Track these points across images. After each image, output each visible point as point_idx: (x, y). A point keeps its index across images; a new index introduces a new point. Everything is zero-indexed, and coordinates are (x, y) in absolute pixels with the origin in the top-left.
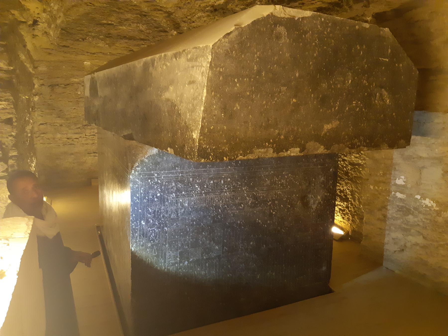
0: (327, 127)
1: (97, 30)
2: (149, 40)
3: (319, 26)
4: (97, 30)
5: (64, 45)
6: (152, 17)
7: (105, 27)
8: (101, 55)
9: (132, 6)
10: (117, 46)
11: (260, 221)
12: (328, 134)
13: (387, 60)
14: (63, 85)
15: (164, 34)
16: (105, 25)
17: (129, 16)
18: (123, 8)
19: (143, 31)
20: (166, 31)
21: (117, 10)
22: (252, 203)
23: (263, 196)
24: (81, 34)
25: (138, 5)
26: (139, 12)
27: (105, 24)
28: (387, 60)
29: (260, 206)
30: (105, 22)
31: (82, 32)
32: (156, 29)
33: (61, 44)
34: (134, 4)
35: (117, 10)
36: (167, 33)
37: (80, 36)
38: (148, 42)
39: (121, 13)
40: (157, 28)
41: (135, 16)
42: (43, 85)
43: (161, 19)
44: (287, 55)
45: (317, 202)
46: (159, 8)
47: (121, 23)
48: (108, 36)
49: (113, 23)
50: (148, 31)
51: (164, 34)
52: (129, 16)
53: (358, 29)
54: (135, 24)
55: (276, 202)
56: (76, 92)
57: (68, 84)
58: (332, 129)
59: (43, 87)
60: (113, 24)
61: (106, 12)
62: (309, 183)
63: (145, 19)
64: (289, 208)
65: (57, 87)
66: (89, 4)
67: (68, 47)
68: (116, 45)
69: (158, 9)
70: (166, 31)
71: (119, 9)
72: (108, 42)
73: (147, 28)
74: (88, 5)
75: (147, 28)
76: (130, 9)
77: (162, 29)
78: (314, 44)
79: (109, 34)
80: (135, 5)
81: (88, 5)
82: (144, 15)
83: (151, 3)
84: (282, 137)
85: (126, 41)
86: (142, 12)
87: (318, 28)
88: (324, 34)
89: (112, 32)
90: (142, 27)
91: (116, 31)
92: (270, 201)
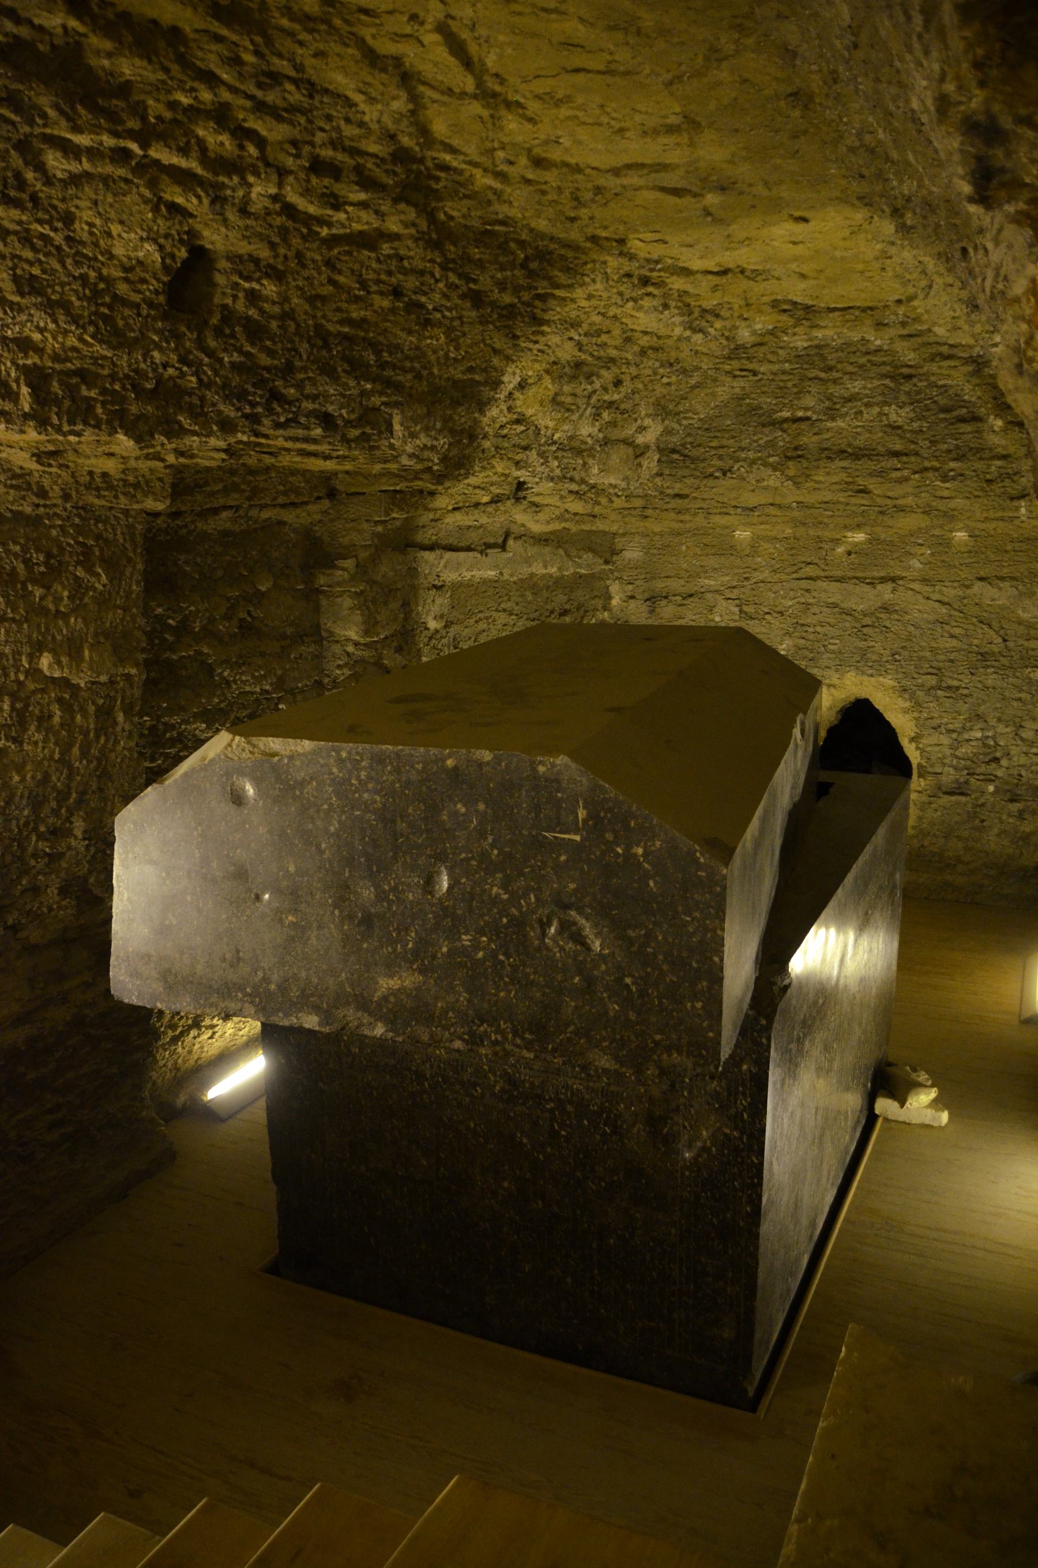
0: (386, 984)
1: (761, 442)
2: (917, 454)
3: (335, 770)
4: (761, 442)
5: (676, 491)
6: (932, 379)
7: (784, 431)
8: (772, 511)
9: (867, 353)
10: (818, 482)
11: (525, 1141)
12: (392, 999)
13: (578, 838)
14: (679, 598)
15: (969, 429)
16: (785, 426)
17: (856, 386)
18: (839, 366)
19: (899, 427)
20: (976, 419)
21: (823, 375)
22: (502, 1090)
23: (532, 1084)
24: (720, 458)
25: (885, 347)
26: (888, 368)
27: (785, 420)
28: (578, 838)
29: (524, 1104)
30: (786, 414)
31: (721, 452)
32: (942, 416)
33: (668, 491)
34: (872, 348)
35: (823, 375)
36: (979, 425)
37: (719, 463)
38: (913, 459)
39: (835, 381)
40: (946, 410)
41: (876, 383)
42: (632, 597)
43: (957, 379)
44: (262, 830)
45: (699, 1144)
46: (945, 349)
47: (831, 413)
48: (795, 454)
49: (809, 414)
50: (915, 425)
51: (969, 429)
52: (856, 386)
53: (456, 768)
54: (877, 410)
55: (569, 1108)
56: (711, 617)
57: (691, 596)
58: (401, 990)
59: (632, 604)
60: (808, 419)
61: (790, 384)
62: (672, 1086)
63: (907, 387)
64: (604, 1133)
65: (664, 602)
66: (738, 373)
67: (687, 496)
68: (816, 478)
69: (941, 354)
70: (976, 419)
71: (830, 369)
72: (791, 473)
73: (912, 415)
74: (735, 377)
75: (912, 415)
76: (861, 366)
77: (964, 411)
78: (326, 807)
79: (796, 449)
80: (876, 351)
81: (735, 377)
82: (901, 375)
83: (919, 340)
84: (273, 987)
85: (845, 464)
86: (897, 367)
87: (331, 773)
88: (352, 785)
89: (804, 440)
90: (897, 415)
91: (815, 439)
92: (551, 1100)
